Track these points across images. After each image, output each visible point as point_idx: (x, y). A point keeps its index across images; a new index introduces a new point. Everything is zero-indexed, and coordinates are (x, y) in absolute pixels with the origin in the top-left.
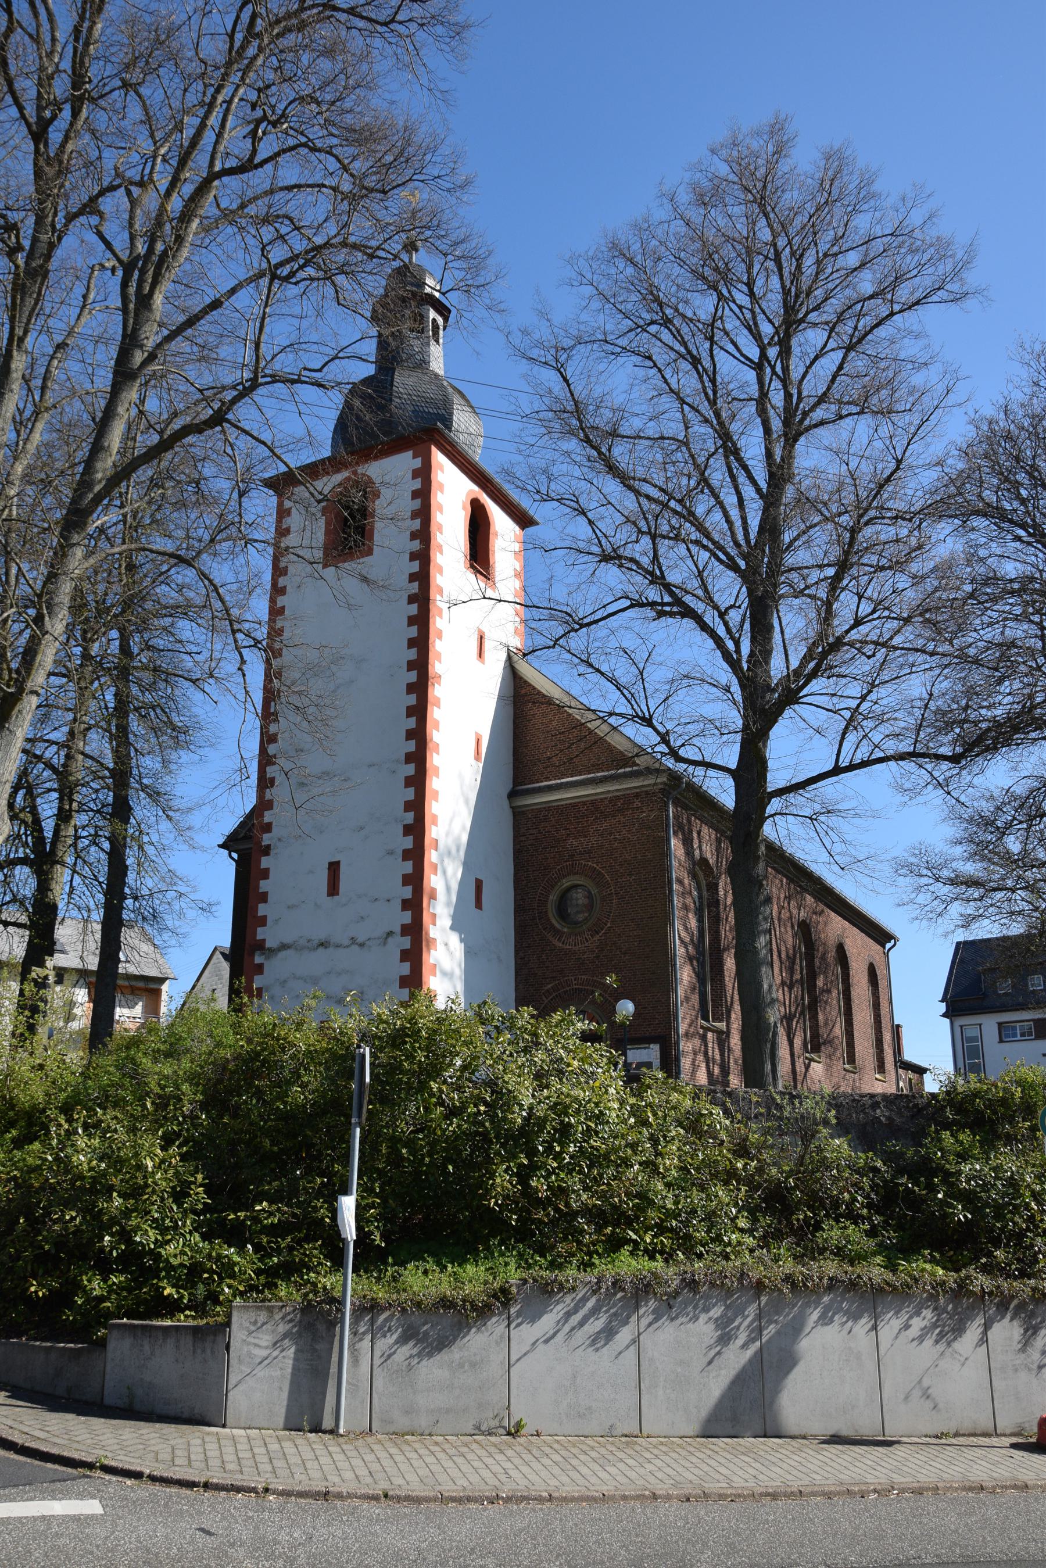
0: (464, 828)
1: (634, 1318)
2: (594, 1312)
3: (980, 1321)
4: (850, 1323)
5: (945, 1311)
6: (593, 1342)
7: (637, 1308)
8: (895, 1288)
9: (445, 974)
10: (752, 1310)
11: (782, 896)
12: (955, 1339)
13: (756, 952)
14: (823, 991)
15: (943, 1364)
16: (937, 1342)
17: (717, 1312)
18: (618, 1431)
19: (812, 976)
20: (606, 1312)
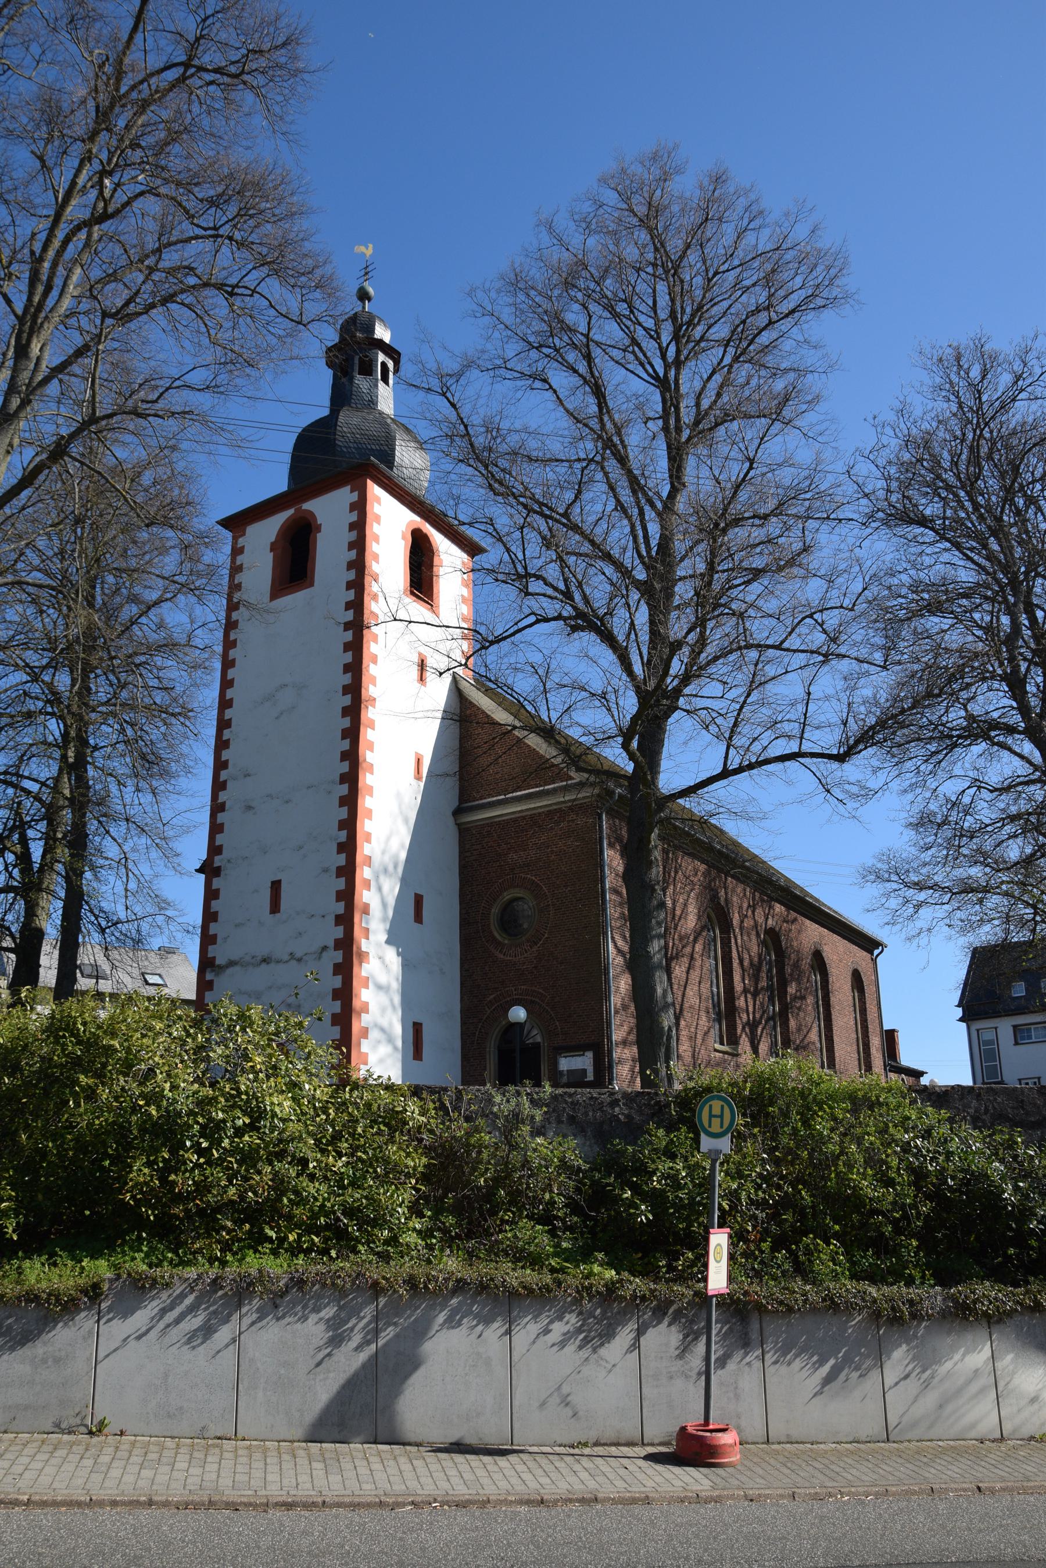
0: (403, 846)
1: (236, 1316)
2: (192, 1309)
3: (632, 1325)
4: (480, 1327)
5: (591, 1314)
6: (189, 1341)
7: (239, 1306)
8: (531, 1291)
9: (379, 987)
10: (368, 1312)
11: (745, 905)
12: (602, 1344)
13: (648, 957)
14: (795, 998)
15: (586, 1371)
16: (580, 1348)
17: (329, 1312)
18: (211, 1433)
19: (783, 984)
20: (205, 1309)
